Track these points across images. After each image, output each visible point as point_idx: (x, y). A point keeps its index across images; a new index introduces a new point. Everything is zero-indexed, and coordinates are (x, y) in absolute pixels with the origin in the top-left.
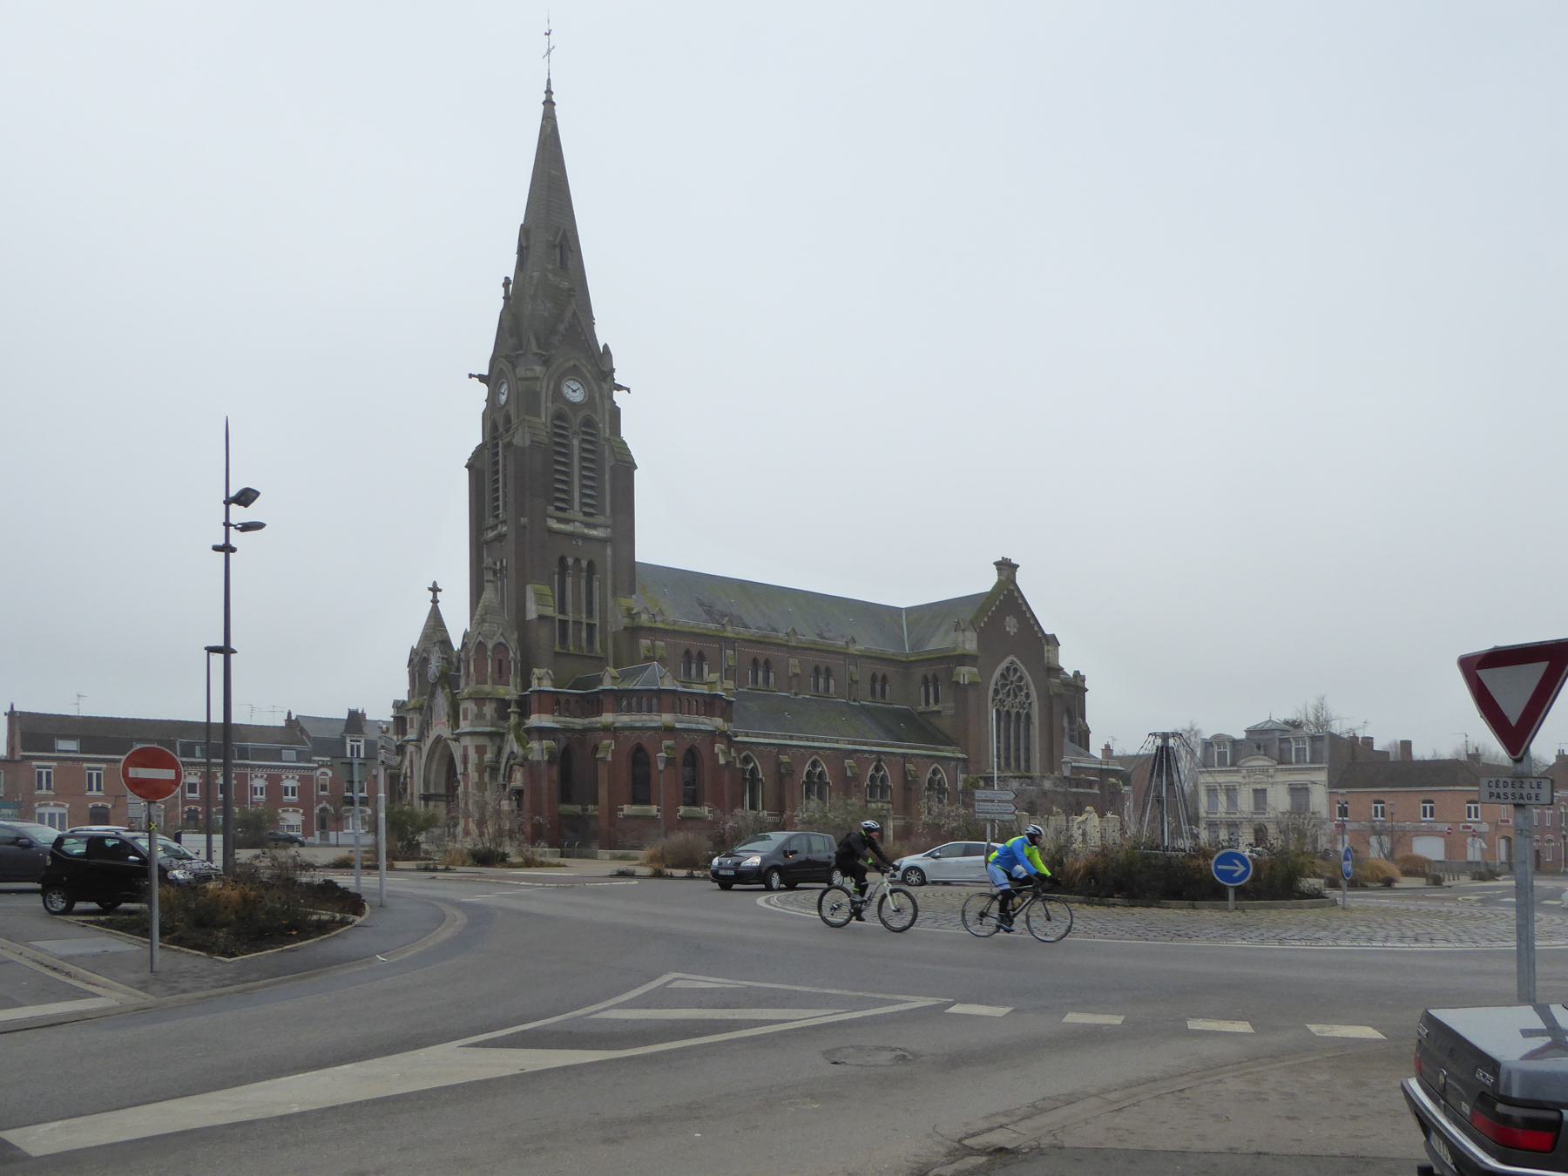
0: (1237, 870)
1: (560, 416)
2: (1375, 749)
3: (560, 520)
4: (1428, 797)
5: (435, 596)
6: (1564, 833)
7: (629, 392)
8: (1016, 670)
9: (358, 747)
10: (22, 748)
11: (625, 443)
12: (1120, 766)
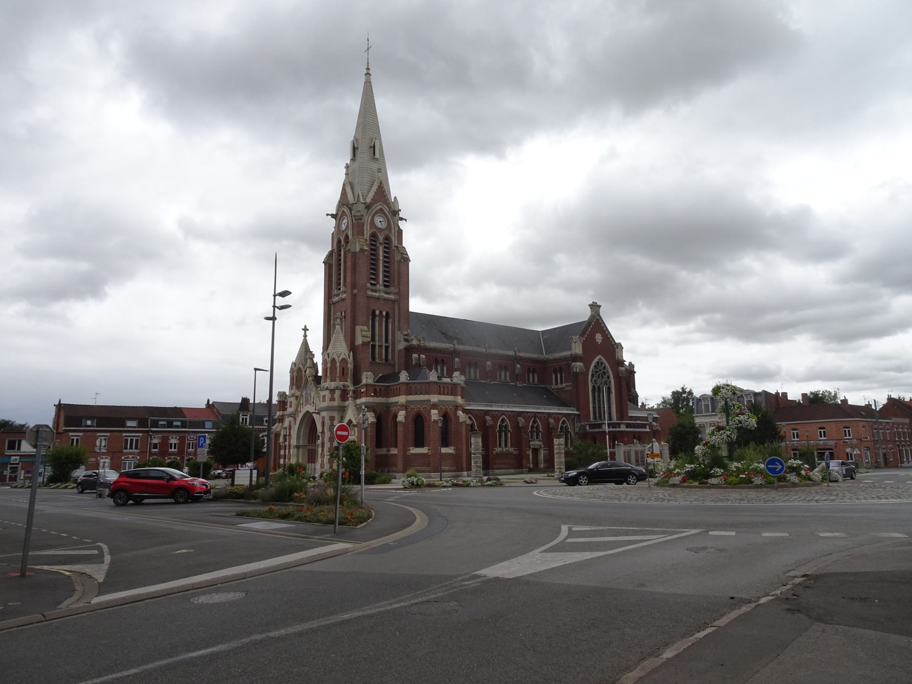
0: (778, 468)
1: (374, 235)
2: (789, 399)
3: (372, 291)
4: (822, 425)
5: (305, 333)
6: (898, 443)
7: (406, 221)
8: (602, 363)
9: (246, 419)
10: (64, 425)
11: (405, 248)
12: (577, 411)
